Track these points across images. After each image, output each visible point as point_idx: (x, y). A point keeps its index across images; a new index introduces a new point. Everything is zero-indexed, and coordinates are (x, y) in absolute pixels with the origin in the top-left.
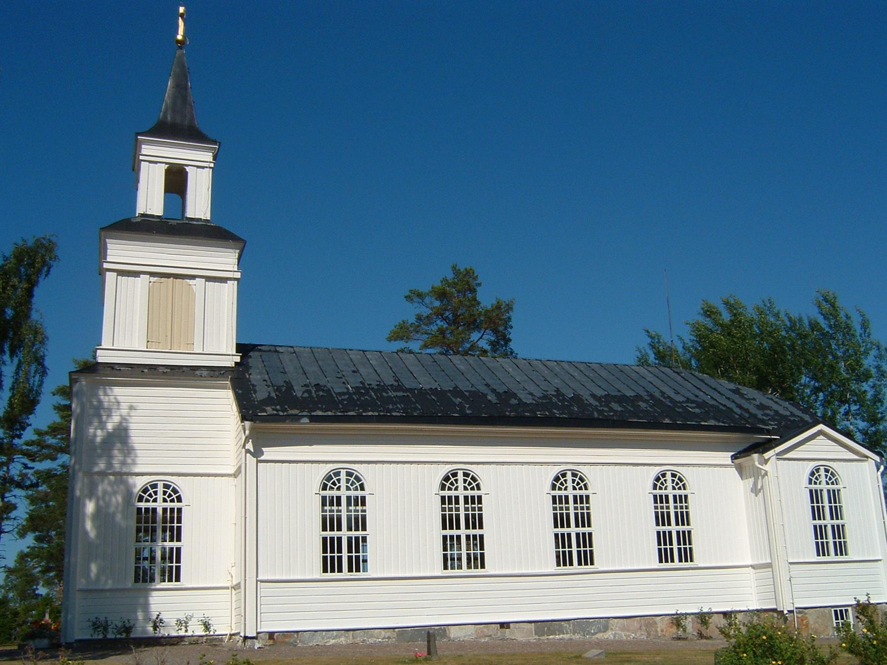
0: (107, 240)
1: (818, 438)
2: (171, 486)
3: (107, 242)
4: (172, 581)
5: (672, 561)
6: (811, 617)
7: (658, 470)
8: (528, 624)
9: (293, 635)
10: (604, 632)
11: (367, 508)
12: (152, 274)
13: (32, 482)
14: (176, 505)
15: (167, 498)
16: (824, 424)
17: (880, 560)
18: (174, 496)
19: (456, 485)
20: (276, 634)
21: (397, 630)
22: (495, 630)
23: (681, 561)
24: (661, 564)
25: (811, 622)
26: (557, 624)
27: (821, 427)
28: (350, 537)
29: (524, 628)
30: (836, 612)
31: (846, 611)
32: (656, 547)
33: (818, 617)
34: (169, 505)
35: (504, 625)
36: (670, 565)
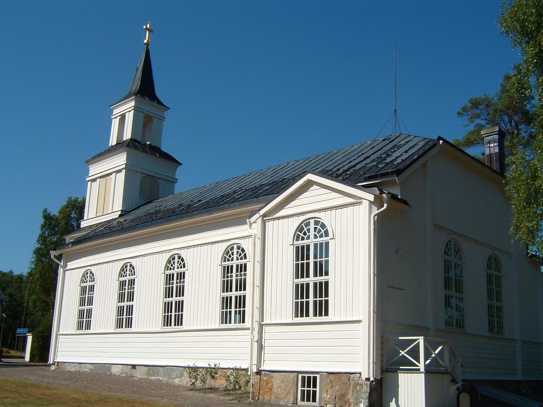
0: (124, 139)
1: (311, 189)
2: (320, 221)
3: (125, 139)
4: (179, 325)
5: (230, 323)
6: (277, 380)
7: (225, 245)
8: (145, 367)
9: (64, 364)
10: (180, 378)
11: (185, 280)
12: (101, 177)
13: (506, 156)
14: (324, 239)
15: (317, 234)
16: (311, 173)
17: (360, 321)
18: (323, 231)
19: (308, 234)
20: (60, 363)
21: (94, 365)
22: (128, 369)
23: (315, 315)
24: (222, 325)
25: (275, 387)
26: (157, 369)
27: (310, 177)
28: (316, 277)
29: (142, 370)
30: (303, 378)
31: (315, 378)
32: (330, 298)
33: (282, 382)
34: (319, 240)
35: (134, 366)
36: (305, 319)
